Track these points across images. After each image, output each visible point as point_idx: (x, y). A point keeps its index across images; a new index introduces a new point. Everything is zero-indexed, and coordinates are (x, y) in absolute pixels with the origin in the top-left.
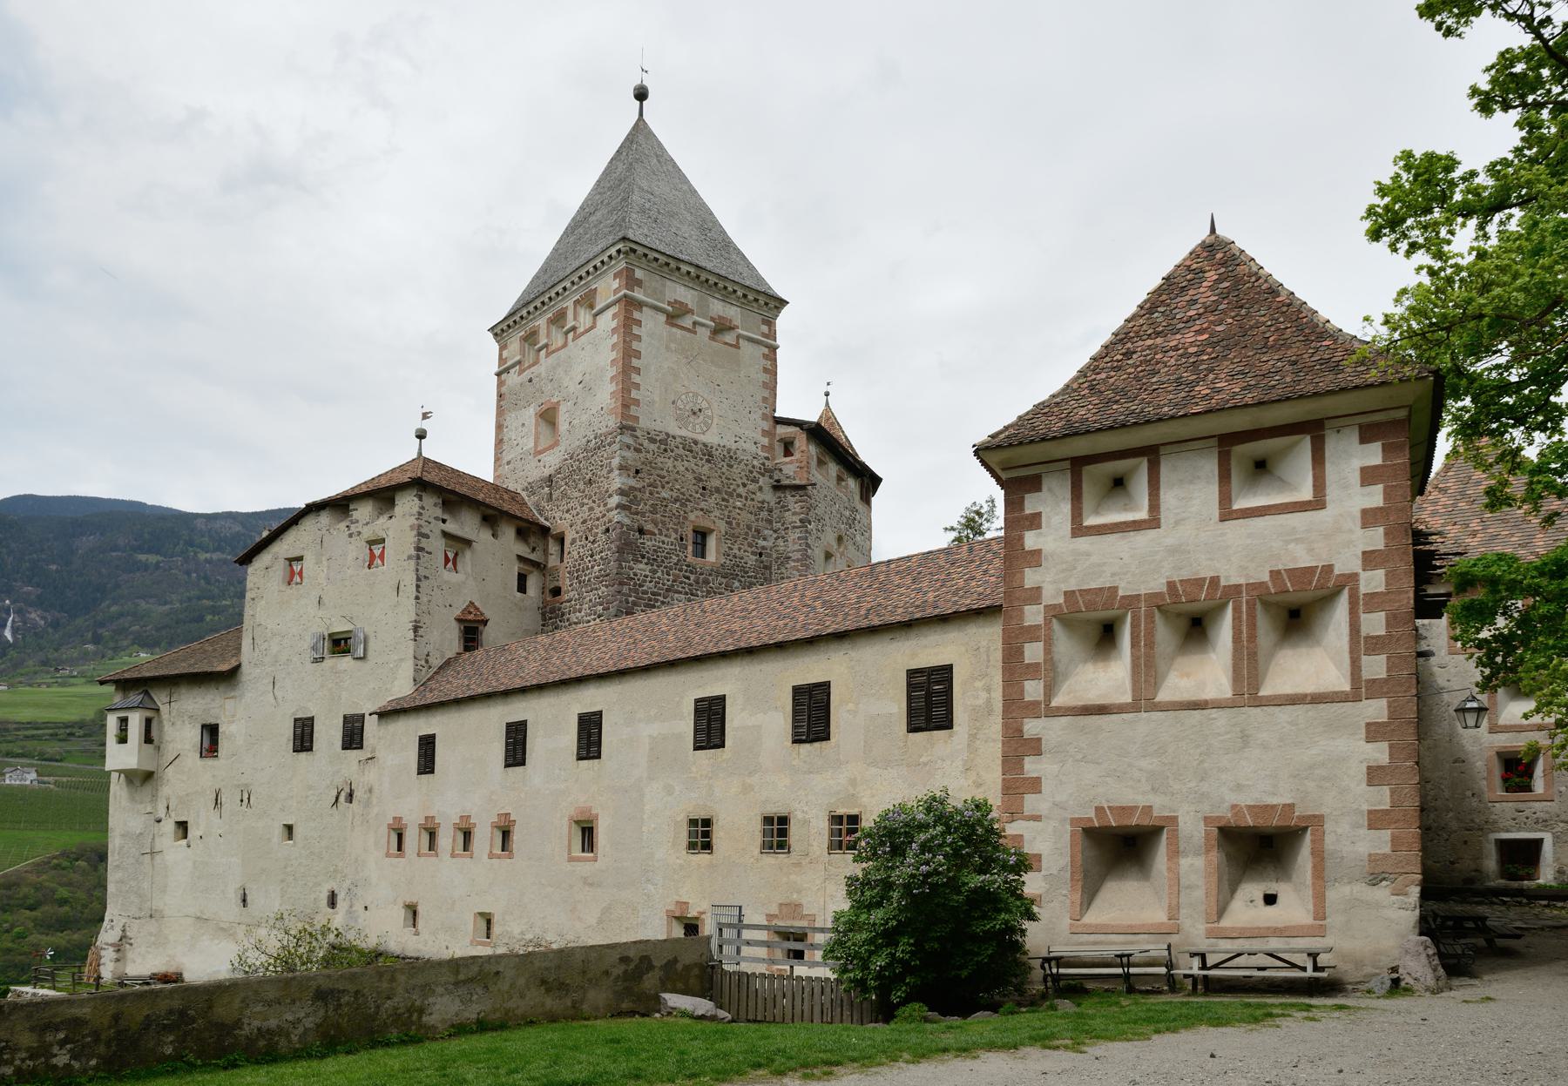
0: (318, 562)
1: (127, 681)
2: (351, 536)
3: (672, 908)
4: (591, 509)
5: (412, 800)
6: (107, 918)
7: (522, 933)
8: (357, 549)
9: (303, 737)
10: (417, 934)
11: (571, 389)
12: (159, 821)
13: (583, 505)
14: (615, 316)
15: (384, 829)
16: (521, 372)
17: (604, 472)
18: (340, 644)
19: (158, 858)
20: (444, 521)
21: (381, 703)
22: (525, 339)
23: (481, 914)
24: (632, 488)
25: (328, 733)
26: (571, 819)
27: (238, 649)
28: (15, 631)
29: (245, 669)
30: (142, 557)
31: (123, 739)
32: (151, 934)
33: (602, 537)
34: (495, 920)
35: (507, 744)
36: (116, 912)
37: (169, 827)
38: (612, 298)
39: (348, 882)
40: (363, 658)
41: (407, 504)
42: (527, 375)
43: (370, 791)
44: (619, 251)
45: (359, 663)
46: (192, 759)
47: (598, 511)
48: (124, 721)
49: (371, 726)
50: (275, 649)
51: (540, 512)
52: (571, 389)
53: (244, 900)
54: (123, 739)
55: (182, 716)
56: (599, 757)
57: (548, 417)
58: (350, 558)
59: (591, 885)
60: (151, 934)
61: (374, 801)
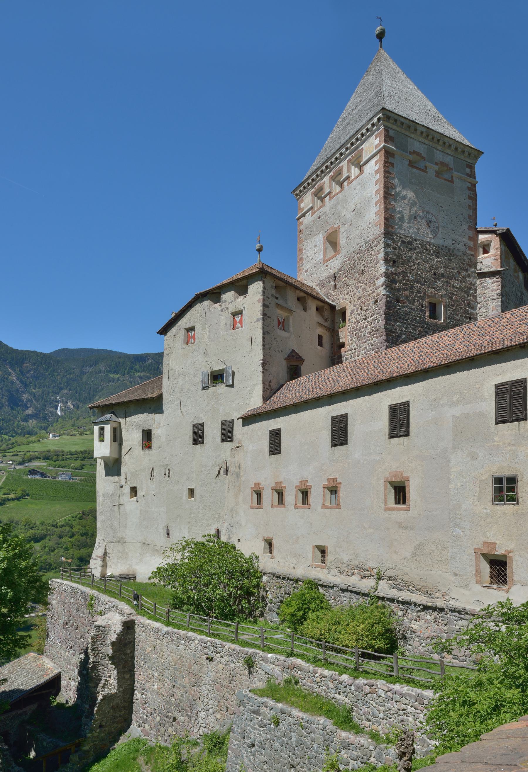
0: (204, 329)
1: (103, 406)
2: (222, 310)
3: (480, 547)
4: (364, 289)
5: (266, 472)
6: (97, 542)
7: (350, 560)
8: (225, 319)
9: (198, 436)
10: (273, 558)
11: (347, 216)
12: (122, 487)
13: (358, 288)
14: (376, 163)
15: (248, 491)
16: (313, 214)
17: (373, 264)
18: (217, 377)
19: (122, 508)
20: (277, 298)
21: (244, 412)
22: (316, 194)
23: (318, 547)
24: (392, 273)
25: (212, 433)
26: (386, 480)
27: (161, 385)
28: (61, 410)
29: (164, 397)
30: (112, 376)
31: (102, 439)
32: (119, 552)
33: (372, 307)
34: (329, 551)
35: (333, 431)
36: (101, 539)
37: (127, 490)
38: (375, 151)
39: (227, 524)
40: (232, 386)
41: (256, 289)
42: (316, 215)
43: (239, 467)
44: (379, 119)
45: (230, 389)
46: (138, 450)
47: (369, 291)
48: (102, 429)
49: (238, 428)
50: (181, 383)
51: (328, 297)
52: (347, 216)
53: (168, 534)
54: (102, 439)
55: (132, 427)
56: (408, 435)
57: (332, 241)
58: (222, 324)
59: (405, 528)
60: (119, 552)
61: (242, 474)
